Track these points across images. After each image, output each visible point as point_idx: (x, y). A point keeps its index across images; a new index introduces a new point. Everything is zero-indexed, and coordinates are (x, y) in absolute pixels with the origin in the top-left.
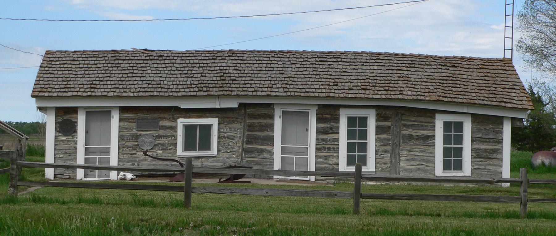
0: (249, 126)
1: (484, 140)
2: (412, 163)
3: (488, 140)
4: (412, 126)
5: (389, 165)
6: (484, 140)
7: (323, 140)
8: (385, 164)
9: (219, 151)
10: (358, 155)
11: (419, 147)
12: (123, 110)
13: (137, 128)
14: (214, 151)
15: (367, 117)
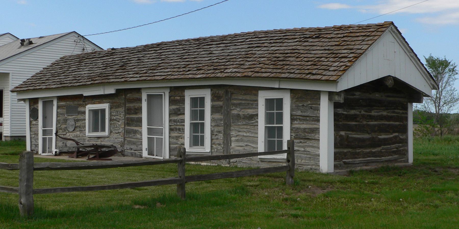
0: (128, 110)
1: (305, 119)
2: (241, 144)
3: (308, 118)
4: (240, 104)
5: (222, 146)
6: (304, 118)
7: (175, 121)
8: (219, 144)
9: (111, 132)
10: (275, 140)
11: (245, 127)
12: (60, 98)
13: (67, 113)
14: (106, 133)
15: (204, 97)
